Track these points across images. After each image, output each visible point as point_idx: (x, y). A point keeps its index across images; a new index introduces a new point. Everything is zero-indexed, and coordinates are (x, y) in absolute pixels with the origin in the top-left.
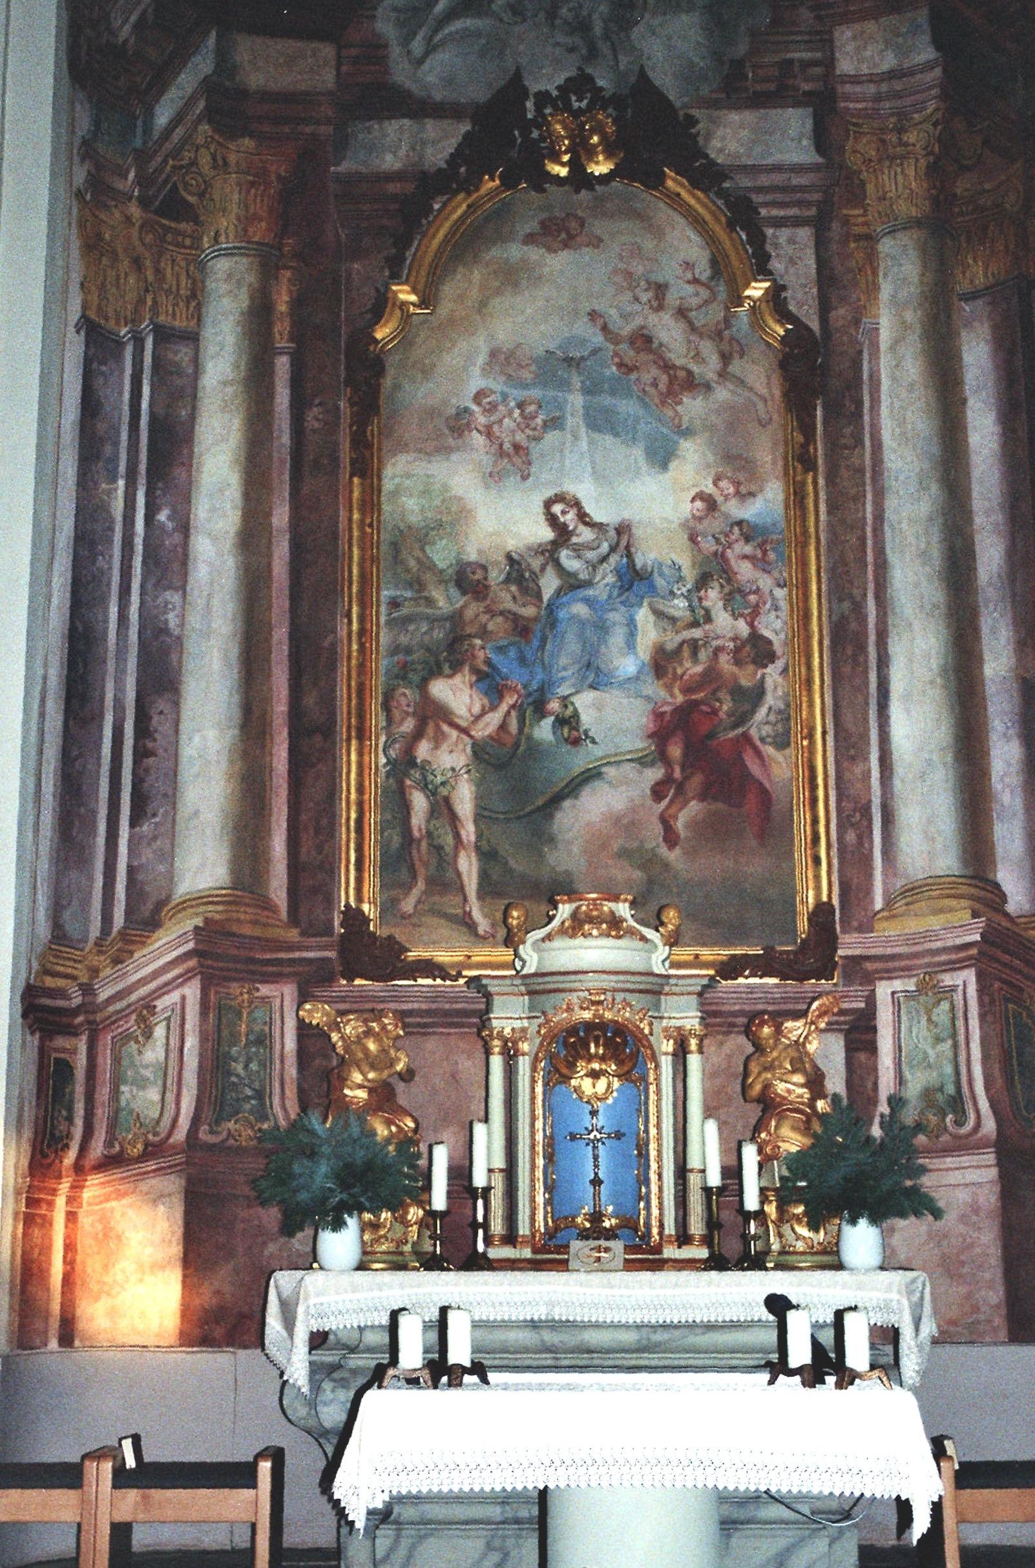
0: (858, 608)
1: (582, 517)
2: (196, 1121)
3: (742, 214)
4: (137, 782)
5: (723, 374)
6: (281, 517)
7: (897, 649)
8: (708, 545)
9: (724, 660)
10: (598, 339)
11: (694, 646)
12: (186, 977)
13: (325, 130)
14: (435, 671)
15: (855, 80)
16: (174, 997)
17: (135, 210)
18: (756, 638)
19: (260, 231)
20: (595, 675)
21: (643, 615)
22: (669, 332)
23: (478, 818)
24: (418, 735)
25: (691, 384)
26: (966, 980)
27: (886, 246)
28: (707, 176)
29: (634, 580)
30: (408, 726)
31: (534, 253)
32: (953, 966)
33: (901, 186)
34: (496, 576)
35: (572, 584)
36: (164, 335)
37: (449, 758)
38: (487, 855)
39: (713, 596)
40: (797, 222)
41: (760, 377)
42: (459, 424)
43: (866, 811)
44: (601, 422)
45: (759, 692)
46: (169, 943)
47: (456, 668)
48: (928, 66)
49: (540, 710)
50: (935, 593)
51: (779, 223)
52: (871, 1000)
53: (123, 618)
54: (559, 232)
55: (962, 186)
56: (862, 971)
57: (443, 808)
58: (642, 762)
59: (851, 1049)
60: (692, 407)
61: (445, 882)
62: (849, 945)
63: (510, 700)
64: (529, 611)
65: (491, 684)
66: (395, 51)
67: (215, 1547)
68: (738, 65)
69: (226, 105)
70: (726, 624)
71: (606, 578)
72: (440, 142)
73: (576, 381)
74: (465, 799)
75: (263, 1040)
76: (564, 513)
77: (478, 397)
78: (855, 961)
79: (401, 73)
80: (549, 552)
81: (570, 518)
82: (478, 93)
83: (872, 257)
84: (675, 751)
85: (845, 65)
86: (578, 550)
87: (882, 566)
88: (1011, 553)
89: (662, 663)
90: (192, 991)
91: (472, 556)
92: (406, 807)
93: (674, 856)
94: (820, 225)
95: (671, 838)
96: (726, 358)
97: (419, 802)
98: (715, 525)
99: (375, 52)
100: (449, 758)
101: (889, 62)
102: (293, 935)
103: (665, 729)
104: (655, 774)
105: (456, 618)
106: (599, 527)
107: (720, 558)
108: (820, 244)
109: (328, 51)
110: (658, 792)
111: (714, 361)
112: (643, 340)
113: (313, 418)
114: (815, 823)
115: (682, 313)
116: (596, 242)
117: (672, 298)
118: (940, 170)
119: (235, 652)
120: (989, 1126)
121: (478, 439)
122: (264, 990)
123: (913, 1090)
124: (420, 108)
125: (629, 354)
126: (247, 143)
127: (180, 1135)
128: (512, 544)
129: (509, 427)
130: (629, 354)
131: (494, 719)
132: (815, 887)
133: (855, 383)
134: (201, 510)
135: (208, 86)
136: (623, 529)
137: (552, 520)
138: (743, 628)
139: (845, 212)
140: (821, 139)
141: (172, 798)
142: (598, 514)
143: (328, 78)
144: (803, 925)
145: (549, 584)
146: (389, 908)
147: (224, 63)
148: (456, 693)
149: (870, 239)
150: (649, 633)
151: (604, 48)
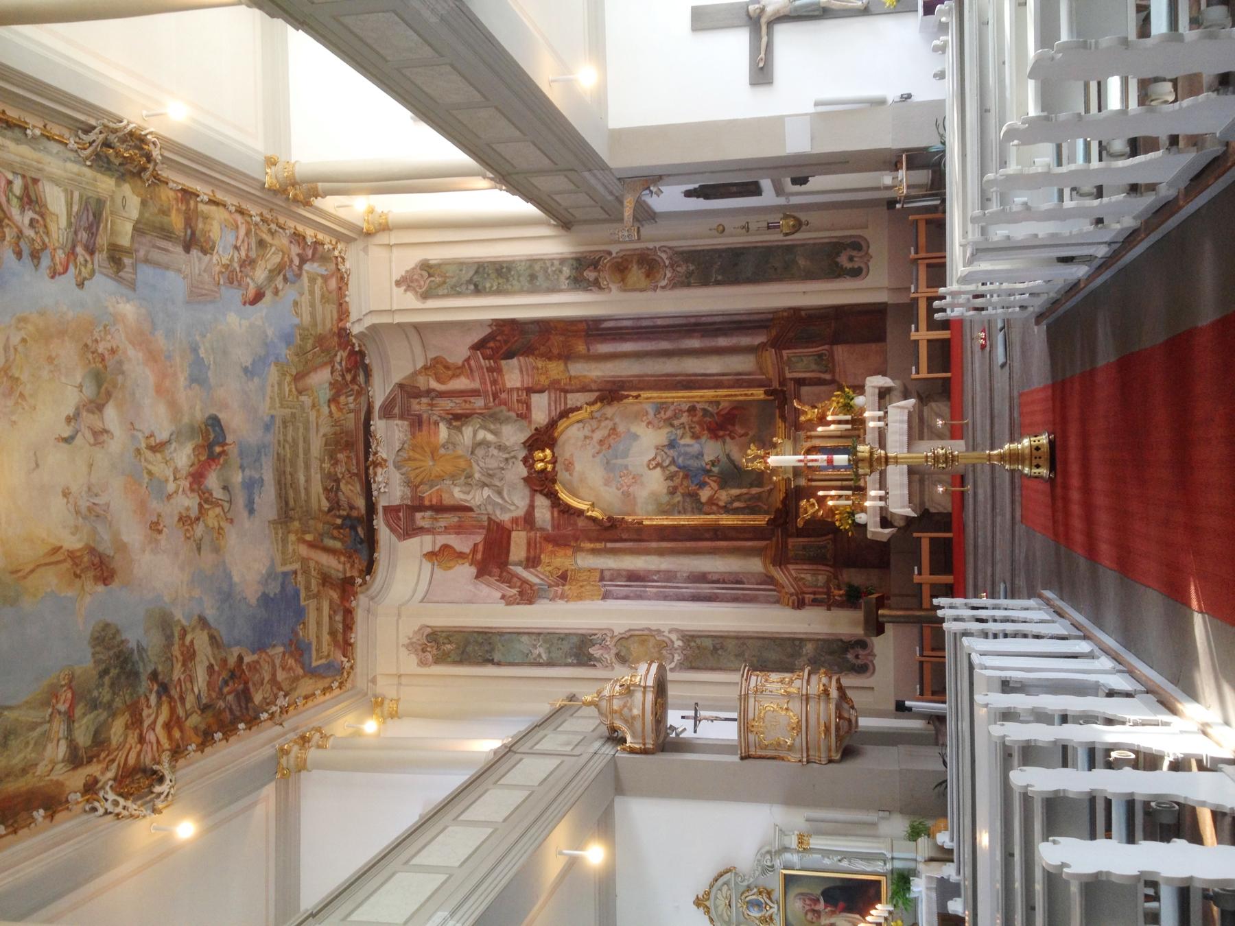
0: (680, 382)
1: (654, 459)
3: (564, 414)
4: (732, 583)
5: (611, 419)
7: (691, 371)
8: (662, 424)
9: (695, 419)
10: (601, 455)
11: (691, 428)
12: (788, 570)
14: (698, 501)
18: (689, 411)
19: (569, 552)
20: (700, 455)
21: (682, 442)
22: (598, 435)
25: (614, 429)
26: (785, 353)
27: (573, 373)
28: (553, 424)
29: (672, 445)
30: (714, 508)
31: (575, 474)
32: (781, 357)
33: (555, 370)
34: (671, 484)
35: (673, 462)
36: (602, 579)
37: (724, 496)
38: (751, 486)
39: (676, 423)
40: (566, 398)
41: (610, 411)
42: (626, 495)
44: (625, 454)
45: (704, 410)
46: (777, 573)
49: (710, 471)
50: (675, 360)
51: (566, 404)
54: (569, 466)
55: (555, 351)
56: (783, 382)
57: (738, 498)
59: (805, 385)
61: (758, 497)
62: (776, 385)
65: (702, 485)
67: (555, 95)
68: (518, 415)
70: (685, 419)
71: (672, 453)
72: (542, 502)
75: (804, 548)
78: (781, 384)
79: (520, 513)
80: (664, 468)
81: (654, 463)
82: (527, 492)
84: (721, 433)
85: (518, 385)
86: (663, 461)
88: (663, 339)
89: (696, 437)
90: (791, 567)
91: (665, 491)
92: (737, 509)
93: (751, 433)
94: (566, 392)
95: (746, 434)
97: (736, 504)
99: (515, 521)
100: (724, 496)
101: (517, 371)
102: (774, 539)
103: (715, 436)
104: (728, 439)
105: (683, 495)
107: (665, 420)
108: (572, 392)
109: (514, 534)
110: (733, 438)
112: (601, 442)
113: (624, 536)
115: (593, 431)
117: (588, 434)
118: (549, 357)
119: (693, 557)
120: (826, 347)
121: (631, 489)
123: (814, 367)
124: (532, 507)
125: (606, 446)
128: (662, 479)
129: (627, 480)
130: (606, 446)
131: (713, 484)
132: (759, 394)
133: (614, 382)
134: (653, 567)
135: (526, 567)
137: (654, 468)
140: (541, 391)
141: (737, 574)
146: (766, 513)
147: (519, 564)
148: (705, 495)
150: (687, 440)
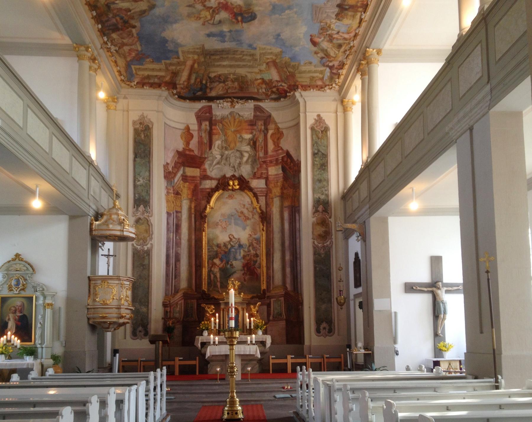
1: (234, 237)
2: (184, 318)
3: (255, 195)
4: (175, 274)
5: (253, 217)
6: (193, 237)
8: (250, 241)
9: (252, 257)
10: (236, 212)
11: (248, 255)
12: (182, 299)
13: (198, 182)
14: (214, 258)
15: (271, 175)
16: (180, 302)
17: (172, 195)
19: (190, 197)
21: (242, 251)
23: (220, 278)
24: (212, 267)
25: (248, 219)
28: (251, 189)
29: (240, 246)
30: (211, 266)
31: (227, 200)
32: (280, 297)
33: (276, 191)
34: (222, 245)
36: (177, 212)
37: (216, 270)
39: (251, 248)
40: (262, 196)
41: (257, 217)
42: (217, 224)
43: (270, 277)
44: (236, 224)
46: (179, 295)
47: (217, 258)
48: (281, 174)
49: (228, 263)
51: (260, 196)
52: (270, 301)
53: (173, 252)
54: (231, 197)
56: (269, 298)
57: (215, 276)
58: (241, 270)
60: (248, 222)
61: (215, 286)
62: (268, 294)
63: (224, 262)
64: (227, 250)
65: (221, 260)
66: (208, 170)
68: (255, 173)
69: (185, 178)
70: (253, 252)
71: (237, 245)
72: (214, 184)
73: (233, 218)
74: (218, 275)
76: (140, 331)
77: (220, 221)
79: (209, 173)
80: (229, 242)
81: (232, 237)
82: (218, 176)
83: (273, 201)
84: (246, 269)
85: (270, 173)
86: (233, 242)
87: (273, 244)
89: (244, 257)
90: (183, 301)
93: (245, 283)
94: (266, 196)
95: (245, 280)
96: (253, 215)
98: (251, 238)
99: (205, 170)
100: (216, 270)
102: (196, 293)
104: (243, 272)
105: (217, 251)
106: (236, 239)
108: (266, 199)
109: (198, 170)
110: (243, 274)
111: (251, 216)
112: (242, 213)
114: (264, 278)
115: (247, 209)
116: (236, 198)
117: (246, 207)
118: (283, 188)
120: (285, 317)
122: (192, 301)
124: (211, 179)
126: (188, 183)
127: (181, 320)
128: (224, 241)
129: (224, 225)
130: (240, 215)
132: (264, 287)
133: (270, 219)
134: (182, 236)
135: (182, 175)
136: (239, 239)
137: (230, 238)
138: (255, 252)
139: (197, 358)
140: (266, 184)
141: (180, 276)
142: (236, 237)
143: (198, 174)
144: (262, 293)
145: (229, 246)
147: (184, 172)
148: (217, 261)
149: (272, 198)
150: (242, 253)
151: (237, 170)
